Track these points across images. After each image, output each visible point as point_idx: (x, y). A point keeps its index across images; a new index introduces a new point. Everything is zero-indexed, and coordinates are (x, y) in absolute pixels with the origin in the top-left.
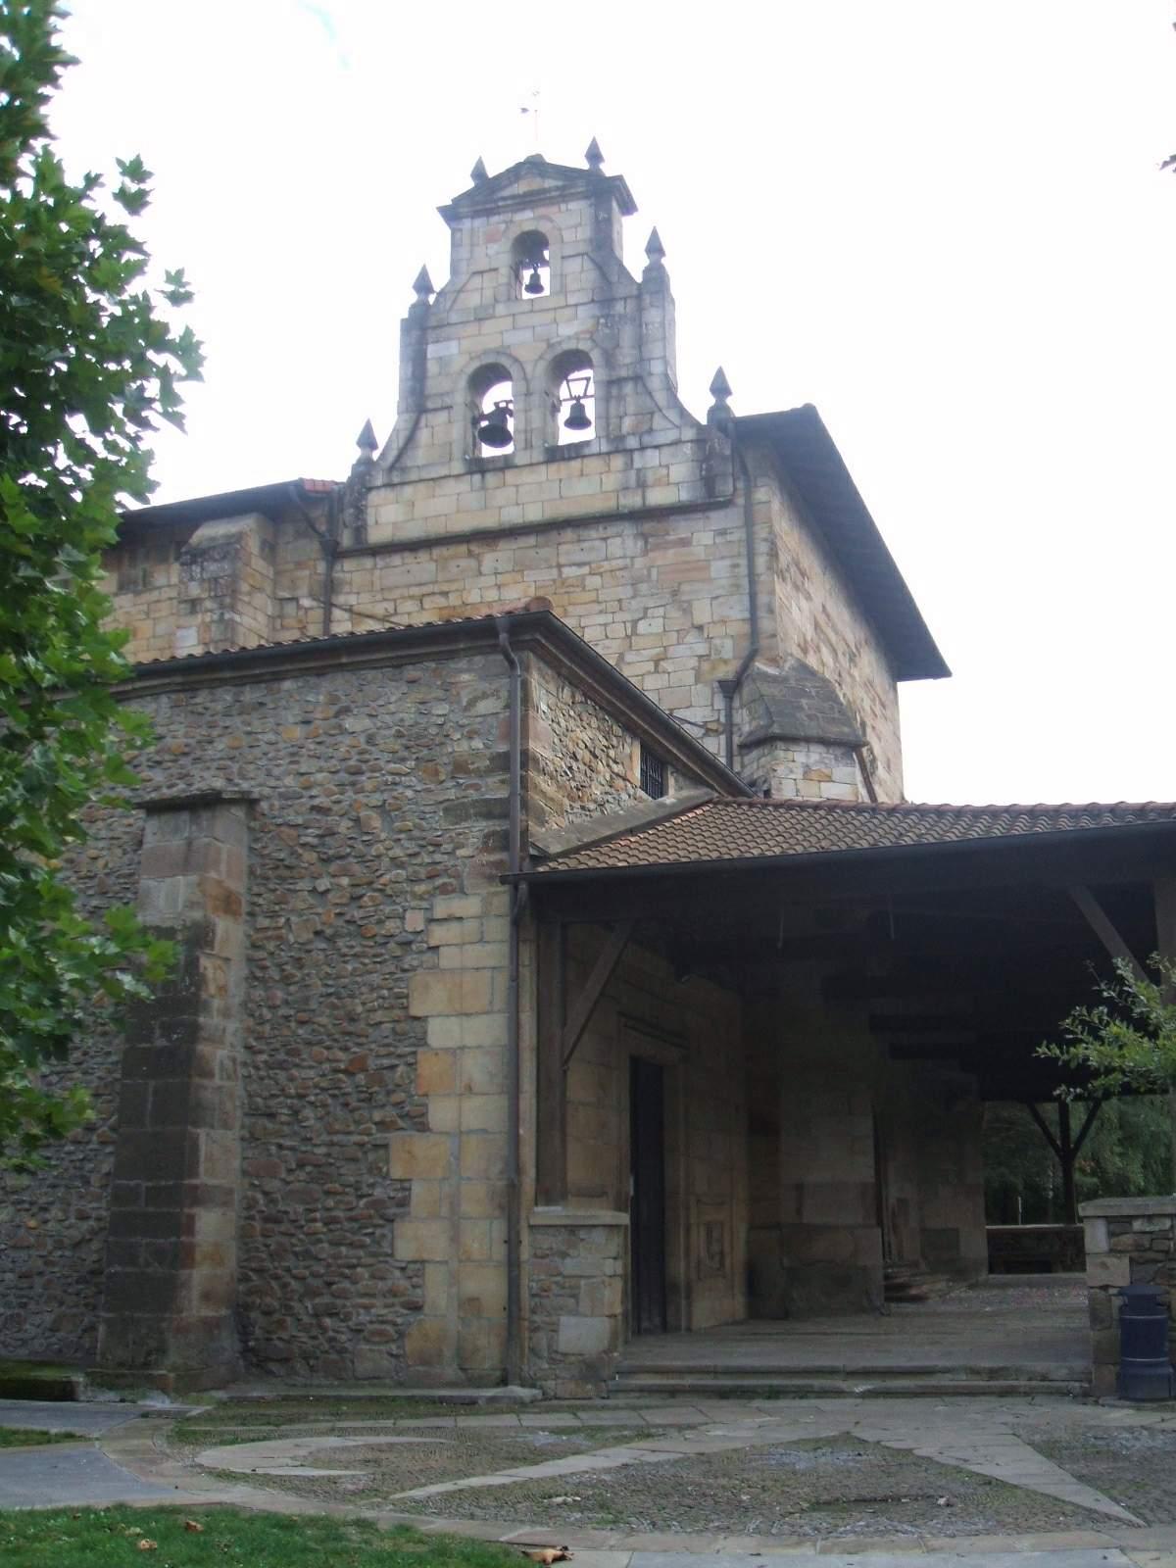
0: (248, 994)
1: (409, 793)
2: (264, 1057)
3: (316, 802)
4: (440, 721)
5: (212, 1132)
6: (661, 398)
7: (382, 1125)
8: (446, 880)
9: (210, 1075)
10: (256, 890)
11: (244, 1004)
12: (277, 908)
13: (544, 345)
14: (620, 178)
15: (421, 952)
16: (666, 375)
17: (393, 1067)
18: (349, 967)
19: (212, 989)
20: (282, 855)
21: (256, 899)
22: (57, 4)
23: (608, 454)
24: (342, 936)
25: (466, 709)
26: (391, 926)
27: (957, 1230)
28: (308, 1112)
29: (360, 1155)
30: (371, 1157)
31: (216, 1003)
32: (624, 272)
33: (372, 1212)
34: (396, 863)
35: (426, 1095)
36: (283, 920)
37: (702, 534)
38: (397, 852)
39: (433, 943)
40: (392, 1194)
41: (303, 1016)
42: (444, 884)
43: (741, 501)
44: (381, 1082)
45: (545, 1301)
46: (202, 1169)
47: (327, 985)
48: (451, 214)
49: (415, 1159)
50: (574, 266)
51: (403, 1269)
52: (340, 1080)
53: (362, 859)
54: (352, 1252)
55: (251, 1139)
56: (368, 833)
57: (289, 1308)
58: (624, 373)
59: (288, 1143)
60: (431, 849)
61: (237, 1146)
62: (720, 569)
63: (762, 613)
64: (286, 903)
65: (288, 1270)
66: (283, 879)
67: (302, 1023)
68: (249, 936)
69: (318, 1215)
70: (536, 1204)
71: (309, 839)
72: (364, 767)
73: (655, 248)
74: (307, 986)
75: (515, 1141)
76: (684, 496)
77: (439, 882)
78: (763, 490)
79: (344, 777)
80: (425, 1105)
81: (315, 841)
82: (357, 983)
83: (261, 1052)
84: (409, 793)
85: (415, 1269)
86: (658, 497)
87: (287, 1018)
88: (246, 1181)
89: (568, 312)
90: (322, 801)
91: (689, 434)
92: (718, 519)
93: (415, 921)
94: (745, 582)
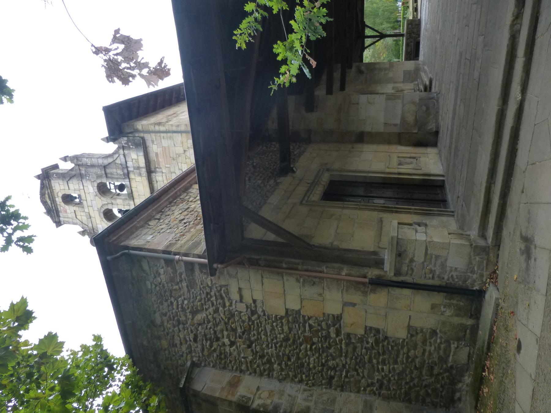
0: (275, 378)
1: (186, 302)
2: (304, 376)
3: (192, 339)
4: (154, 286)
6: (110, 160)
7: (338, 333)
8: (222, 292)
10: (230, 368)
11: (280, 381)
12: (238, 361)
13: (96, 197)
14: (42, 170)
15: (256, 307)
16: (103, 158)
17: (310, 326)
18: (263, 337)
19: (269, 402)
20: (215, 355)
21: (234, 368)
23: (129, 179)
24: (250, 338)
25: (147, 274)
26: (245, 318)
27: (404, 71)
28: (331, 363)
29: (352, 346)
30: (353, 341)
31: (276, 400)
32: (72, 170)
33: (381, 345)
34: (216, 311)
35: (324, 314)
36: (243, 360)
37: (154, 149)
38: (211, 310)
39: (251, 302)
40: (372, 335)
41: (286, 358)
42: (224, 293)
43: (142, 135)
44: (318, 331)
45: (437, 273)
47: (272, 347)
48: (59, 224)
49: (355, 322)
50: (71, 185)
51: (412, 336)
52: (315, 348)
53: (216, 325)
54: (401, 356)
55: (342, 388)
56: (204, 321)
57: (426, 386)
58: (103, 172)
59: (344, 374)
60: (209, 296)
61: (345, 394)
62: (165, 143)
63: (179, 129)
64: (235, 357)
65: (407, 383)
66: (226, 357)
67: (289, 359)
68: (250, 374)
69: (380, 367)
70: (383, 269)
71: (208, 344)
72: (176, 318)
73: (65, 159)
74: (272, 355)
75: (369, 172)
76: (141, 154)
77: (224, 295)
78: (138, 127)
79: (181, 326)
80: (329, 315)
81: (209, 342)
82: (270, 335)
83: (302, 377)
84: (186, 302)
85: (412, 331)
86: (142, 162)
87: (286, 365)
88: (362, 392)
89: (85, 188)
90: (192, 336)
91: (121, 151)
92: (149, 143)
93: (242, 307)
94: (169, 135)
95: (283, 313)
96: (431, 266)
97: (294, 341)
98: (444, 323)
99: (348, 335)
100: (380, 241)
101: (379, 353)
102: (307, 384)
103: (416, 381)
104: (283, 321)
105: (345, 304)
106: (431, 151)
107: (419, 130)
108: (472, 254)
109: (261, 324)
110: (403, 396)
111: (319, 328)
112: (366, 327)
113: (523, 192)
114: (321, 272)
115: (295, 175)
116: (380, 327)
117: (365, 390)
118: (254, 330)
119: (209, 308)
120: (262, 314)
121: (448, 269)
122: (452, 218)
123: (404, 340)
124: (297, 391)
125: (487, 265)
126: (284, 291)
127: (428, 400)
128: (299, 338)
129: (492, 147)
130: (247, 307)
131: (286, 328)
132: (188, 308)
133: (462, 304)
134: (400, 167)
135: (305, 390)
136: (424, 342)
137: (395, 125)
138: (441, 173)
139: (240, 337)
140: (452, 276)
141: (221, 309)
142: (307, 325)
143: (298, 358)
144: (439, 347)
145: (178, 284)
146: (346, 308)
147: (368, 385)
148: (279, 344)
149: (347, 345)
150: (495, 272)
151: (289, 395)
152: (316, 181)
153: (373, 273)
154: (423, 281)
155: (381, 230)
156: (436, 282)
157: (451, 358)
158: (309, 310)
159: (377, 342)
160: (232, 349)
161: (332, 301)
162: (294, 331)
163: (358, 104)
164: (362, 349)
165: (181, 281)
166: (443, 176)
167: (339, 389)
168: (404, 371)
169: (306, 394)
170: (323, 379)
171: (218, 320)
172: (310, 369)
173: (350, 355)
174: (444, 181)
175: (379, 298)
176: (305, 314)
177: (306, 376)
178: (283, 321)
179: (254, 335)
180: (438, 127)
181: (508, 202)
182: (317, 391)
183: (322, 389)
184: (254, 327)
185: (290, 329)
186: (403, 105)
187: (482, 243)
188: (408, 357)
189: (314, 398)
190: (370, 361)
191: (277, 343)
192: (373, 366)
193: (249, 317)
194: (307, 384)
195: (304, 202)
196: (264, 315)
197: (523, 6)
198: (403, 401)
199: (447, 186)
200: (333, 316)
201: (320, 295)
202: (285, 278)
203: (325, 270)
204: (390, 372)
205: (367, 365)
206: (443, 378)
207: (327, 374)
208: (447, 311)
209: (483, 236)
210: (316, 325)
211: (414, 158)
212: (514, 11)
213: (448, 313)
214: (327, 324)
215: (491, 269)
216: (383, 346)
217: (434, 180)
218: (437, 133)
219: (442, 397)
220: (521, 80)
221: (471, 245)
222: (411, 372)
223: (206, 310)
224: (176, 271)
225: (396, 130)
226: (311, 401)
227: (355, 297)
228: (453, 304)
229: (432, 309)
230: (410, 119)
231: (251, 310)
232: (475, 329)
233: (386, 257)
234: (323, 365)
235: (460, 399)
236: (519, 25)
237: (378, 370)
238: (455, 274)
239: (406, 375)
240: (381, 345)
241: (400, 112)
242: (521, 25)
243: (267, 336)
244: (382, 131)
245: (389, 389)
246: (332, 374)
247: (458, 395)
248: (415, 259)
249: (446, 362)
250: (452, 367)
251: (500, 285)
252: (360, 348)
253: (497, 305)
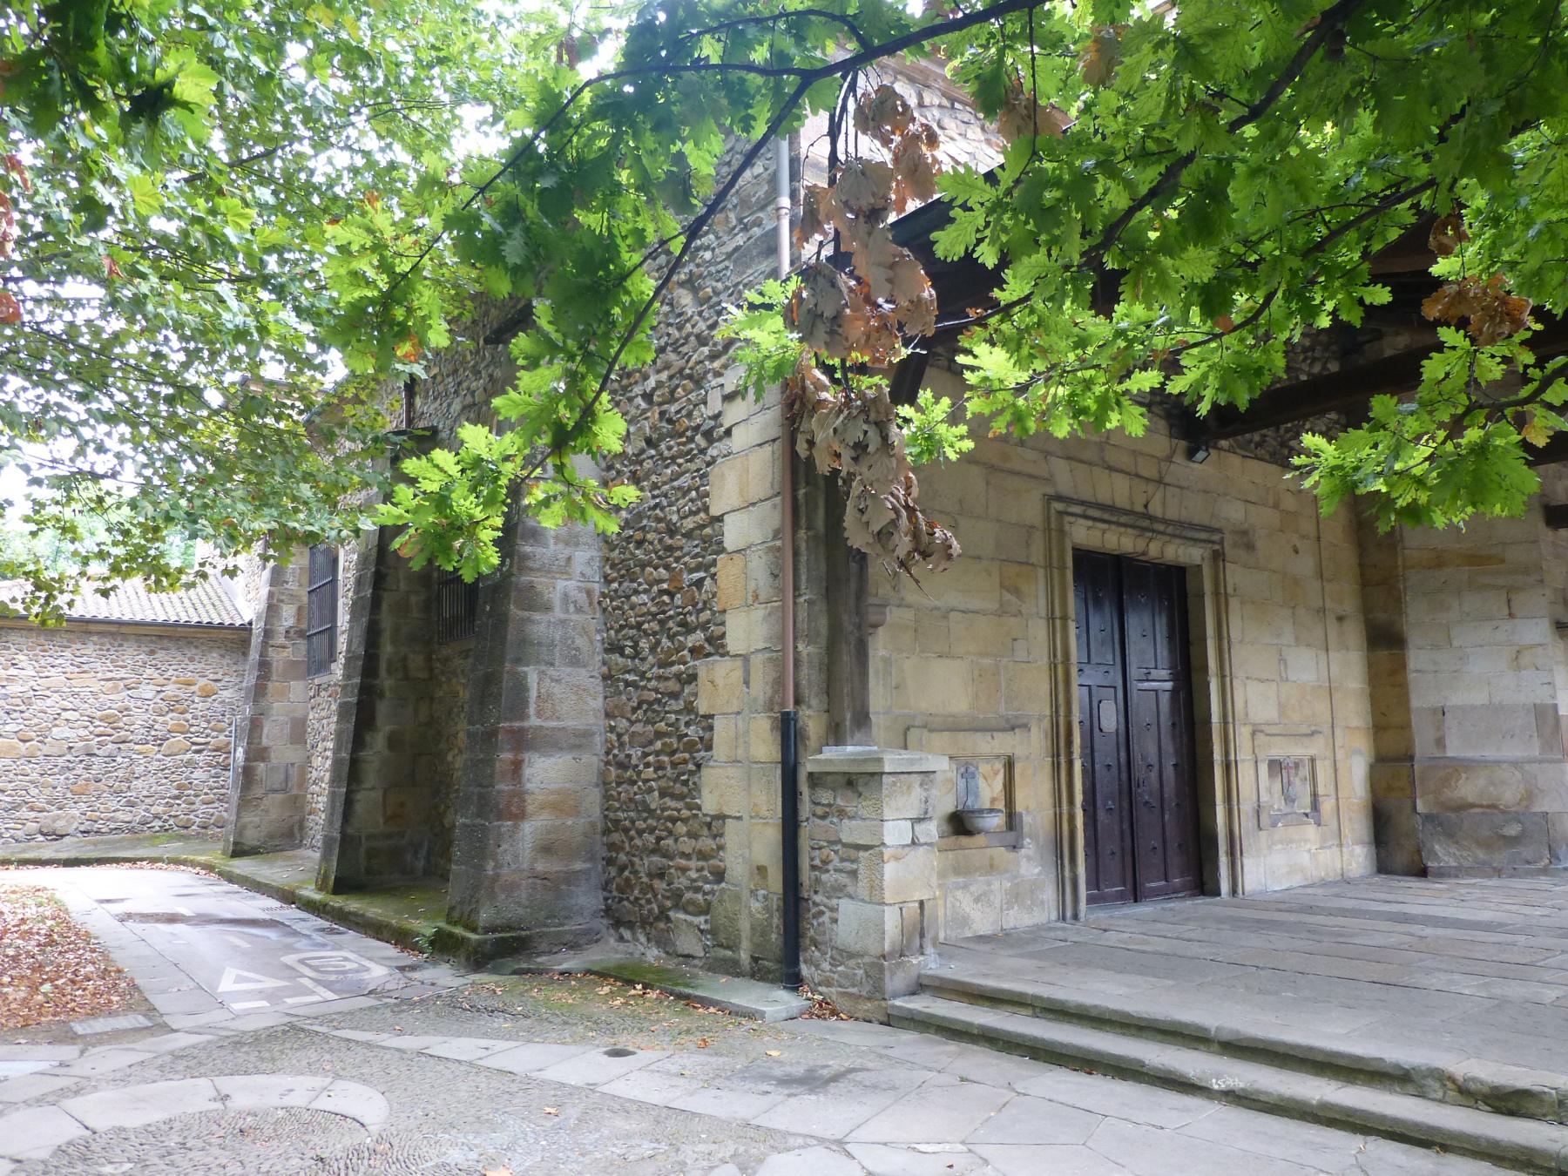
1: (708, 255)
2: (615, 585)
5: (551, 671)
7: (696, 652)
9: (548, 608)
15: (720, 439)
22: (1564, 4)
33: (687, 755)
35: (724, 611)
39: (727, 425)
41: (639, 535)
45: (824, 877)
46: (532, 710)
51: (709, 825)
61: (597, 686)
67: (639, 544)
69: (651, 758)
80: (723, 624)
95: (715, 511)
96: (836, 862)
97: (670, 549)
98: (737, 898)
99: (693, 678)
100: (931, 731)
101: (673, 752)
102: (604, 595)
103: (638, 842)
104: (702, 515)
105: (746, 658)
106: (1357, 857)
107: (1428, 818)
108: (867, 959)
109: (690, 461)
110: (611, 815)
111: (700, 605)
112: (712, 716)
113: (962, 1080)
114: (796, 588)
115: (1179, 459)
116: (714, 752)
117: (612, 729)
118: (679, 444)
119: (705, 320)
120: (708, 458)
121: (834, 902)
122: (1054, 916)
123: (699, 808)
124: (583, 574)
125: (850, 995)
126: (753, 504)
127: (613, 871)
128: (677, 560)
129: (1116, 1012)
130: (716, 417)
131: (689, 524)
132: (698, 266)
133: (774, 936)
134: (1264, 769)
135: (589, 593)
136: (703, 856)
137: (1440, 743)
138: (1247, 888)
139: (662, 414)
140: (821, 913)
141: (706, 350)
142: (702, 574)
143: (643, 566)
144: (697, 890)
145: (740, 220)
146: (739, 662)
147: (619, 736)
148: (661, 515)
149: (678, 676)
150: (834, 1013)
151: (569, 559)
152: (1161, 527)
153: (812, 721)
154: (804, 843)
155: (976, 730)
156: (806, 875)
157: (681, 916)
158: (727, 570)
159: (691, 747)
160: (639, 400)
161: (747, 629)
162: (688, 545)
163: (1511, 615)
164: (676, 712)
165: (746, 229)
166: (1234, 892)
167: (605, 669)
168: (651, 812)
169: (582, 598)
170: (617, 632)
171: (684, 349)
172: (628, 597)
173: (662, 686)
174: (1216, 892)
175: (764, 746)
176: (719, 564)
177: (616, 591)
178: (702, 515)
179: (670, 448)
180: (1442, 874)
181: (975, 1047)
182: (592, 621)
183: (599, 631)
184: (684, 444)
185: (688, 535)
186: (1515, 764)
187: (895, 981)
188: (674, 820)
189: (574, 617)
190: (659, 735)
191: (662, 509)
192: (651, 743)
193: (699, 426)
194: (604, 595)
195: (1059, 506)
196: (708, 464)
197: (1498, 1111)
198: (606, 817)
199: (1202, 904)
200: (723, 635)
201: (756, 597)
202: (778, 499)
203: (802, 600)
204: (646, 781)
205: (650, 727)
206: (649, 902)
207: (626, 638)
208: (758, 905)
209: (921, 987)
210: (704, 597)
211: (1315, 806)
212: (1482, 1083)
213: (756, 906)
214: (708, 622)
215: (842, 1004)
216: (685, 762)
217: (1216, 868)
218: (1422, 873)
219: (621, 900)
220: (1259, 1092)
221: (884, 957)
222: (652, 830)
223: (700, 314)
224: (762, 208)
225: (1423, 746)
226: (567, 611)
227: (760, 687)
228: (771, 916)
229: (759, 868)
230: (1468, 789)
231: (713, 429)
232: (731, 968)
233: (850, 749)
234: (639, 626)
235: (621, 939)
236: (1440, 1095)
237: (645, 755)
238: (825, 918)
239: (645, 820)
240: (687, 755)
241: (1490, 753)
242: (1441, 1101)
243: (672, 480)
244: (1415, 703)
245: (619, 784)
246: (628, 651)
247: (627, 934)
248: (845, 821)
249: (676, 907)
250: (668, 919)
251: (802, 1025)
252: (676, 708)
253: (751, 1015)
